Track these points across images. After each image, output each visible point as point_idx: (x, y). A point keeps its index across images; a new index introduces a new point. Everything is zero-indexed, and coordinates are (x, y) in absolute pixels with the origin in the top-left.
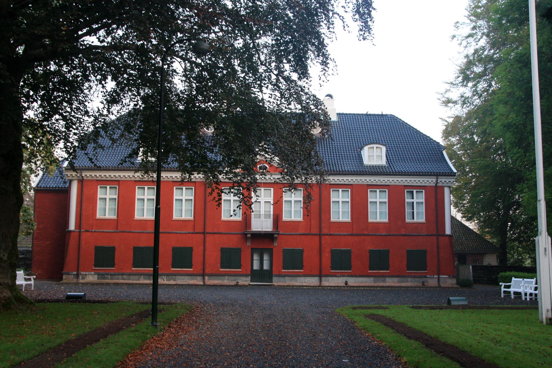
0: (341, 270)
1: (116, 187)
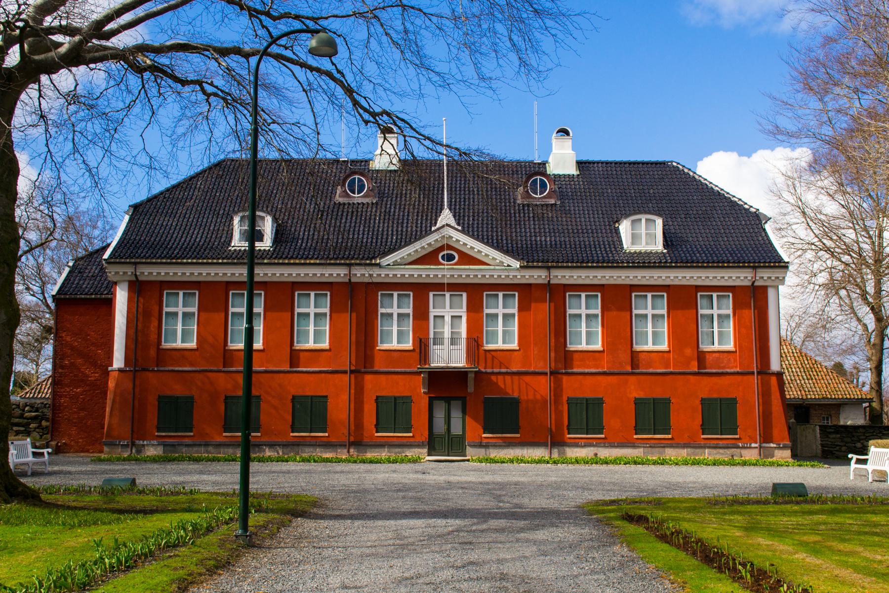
0: (176, 432)
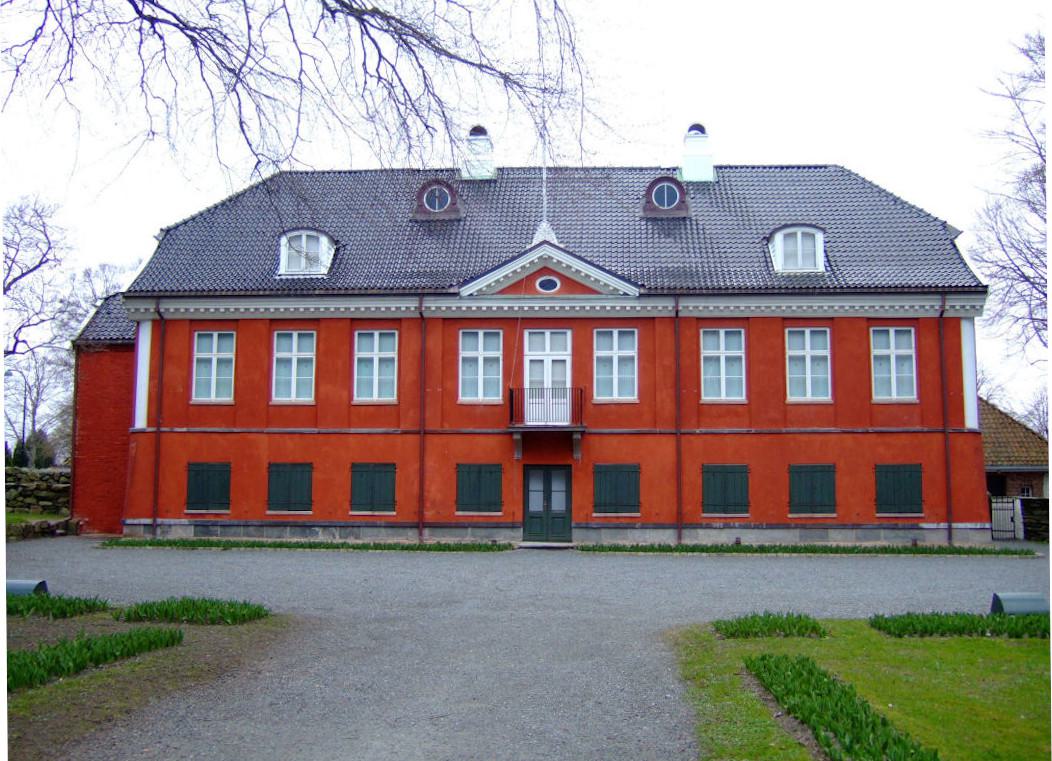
1: (825, 332)
